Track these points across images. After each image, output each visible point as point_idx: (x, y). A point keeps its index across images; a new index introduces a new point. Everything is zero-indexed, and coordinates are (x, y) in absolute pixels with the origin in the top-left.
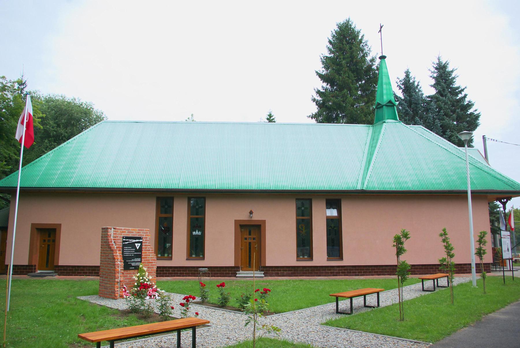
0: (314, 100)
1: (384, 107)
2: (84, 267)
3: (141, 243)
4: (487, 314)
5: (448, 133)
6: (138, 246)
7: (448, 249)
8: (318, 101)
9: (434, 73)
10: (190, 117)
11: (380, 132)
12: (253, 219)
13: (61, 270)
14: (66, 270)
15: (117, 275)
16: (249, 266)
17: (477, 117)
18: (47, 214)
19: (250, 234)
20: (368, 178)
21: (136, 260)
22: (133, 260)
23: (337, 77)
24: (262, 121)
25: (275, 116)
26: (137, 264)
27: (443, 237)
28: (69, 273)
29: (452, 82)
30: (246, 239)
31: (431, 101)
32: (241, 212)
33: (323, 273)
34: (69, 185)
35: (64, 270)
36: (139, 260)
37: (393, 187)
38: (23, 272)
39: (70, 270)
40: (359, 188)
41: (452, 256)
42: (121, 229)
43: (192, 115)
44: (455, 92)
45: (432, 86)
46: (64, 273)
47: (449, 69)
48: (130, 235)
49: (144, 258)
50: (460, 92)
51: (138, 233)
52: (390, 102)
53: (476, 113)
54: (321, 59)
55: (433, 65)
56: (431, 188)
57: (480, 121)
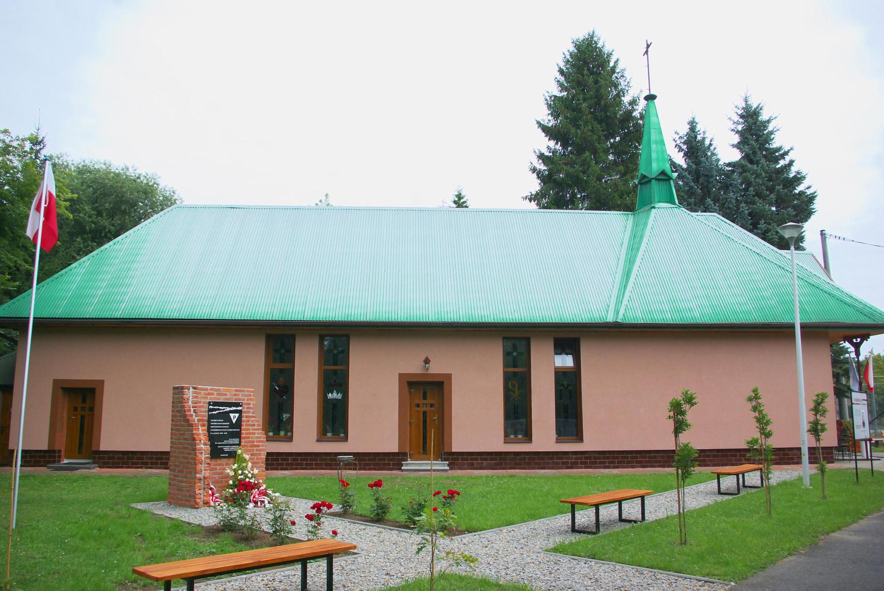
0: (534, 170)
1: (653, 182)
2: (143, 453)
3: (240, 412)
4: (828, 534)
5: (762, 225)
6: (234, 417)
7: (762, 422)
8: (540, 171)
9: (738, 123)
10: (323, 198)
11: (645, 225)
12: (431, 371)
13: (103, 458)
14: (113, 458)
15: (199, 467)
16: (423, 451)
17: (811, 199)
18: (80, 364)
19: (425, 397)
20: (625, 302)
21: (231, 441)
22: (225, 442)
23: (573, 130)
24: (445, 205)
25: (468, 197)
26: (233, 448)
27: (754, 403)
28: (118, 463)
29: (768, 139)
30: (418, 406)
31: (733, 171)
32: (410, 360)
33: (548, 463)
34: (117, 315)
35: (109, 458)
36: (236, 441)
37: (668, 317)
38: (40, 462)
39: (119, 458)
40: (610, 319)
41: (768, 435)
42: (206, 389)
43: (327, 195)
44: (774, 155)
45: (734, 146)
46: (109, 463)
47: (764, 117)
48: (222, 399)
49: (245, 438)
50: (783, 156)
51: (235, 395)
52: (663, 173)
53: (809, 192)
54: (546, 100)
55: (736, 110)
56: (732, 319)
57: (817, 205)
